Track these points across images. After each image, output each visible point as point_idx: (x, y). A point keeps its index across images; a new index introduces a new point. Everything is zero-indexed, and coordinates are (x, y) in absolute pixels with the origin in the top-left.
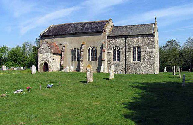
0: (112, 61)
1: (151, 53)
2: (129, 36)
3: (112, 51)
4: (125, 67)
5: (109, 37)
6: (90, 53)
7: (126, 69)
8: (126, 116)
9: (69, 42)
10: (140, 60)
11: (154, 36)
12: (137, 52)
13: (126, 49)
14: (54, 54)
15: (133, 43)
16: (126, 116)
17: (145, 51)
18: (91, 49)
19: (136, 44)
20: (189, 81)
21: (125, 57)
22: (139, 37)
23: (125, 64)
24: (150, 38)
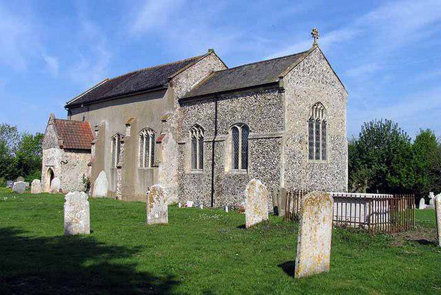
0: (188, 168)
1: (270, 143)
2: (222, 95)
3: (188, 141)
4: (213, 185)
5: (184, 102)
6: (149, 147)
7: (213, 191)
8: (137, 250)
9: (109, 120)
10: (245, 166)
11: (281, 90)
12: (240, 140)
13: (216, 135)
14: (67, 150)
15: (233, 112)
16: (137, 250)
17: (258, 139)
18: (144, 133)
19: (238, 118)
20: (114, 150)
21: (213, 155)
22: (247, 94)
23: (213, 177)
24: (272, 96)
